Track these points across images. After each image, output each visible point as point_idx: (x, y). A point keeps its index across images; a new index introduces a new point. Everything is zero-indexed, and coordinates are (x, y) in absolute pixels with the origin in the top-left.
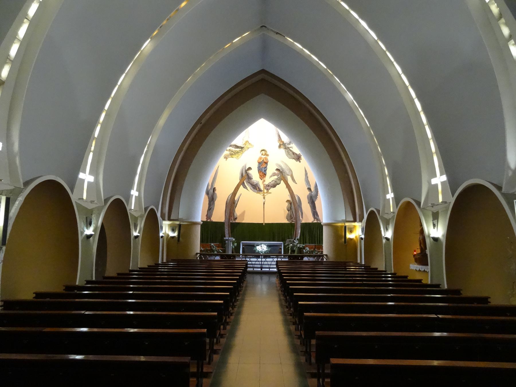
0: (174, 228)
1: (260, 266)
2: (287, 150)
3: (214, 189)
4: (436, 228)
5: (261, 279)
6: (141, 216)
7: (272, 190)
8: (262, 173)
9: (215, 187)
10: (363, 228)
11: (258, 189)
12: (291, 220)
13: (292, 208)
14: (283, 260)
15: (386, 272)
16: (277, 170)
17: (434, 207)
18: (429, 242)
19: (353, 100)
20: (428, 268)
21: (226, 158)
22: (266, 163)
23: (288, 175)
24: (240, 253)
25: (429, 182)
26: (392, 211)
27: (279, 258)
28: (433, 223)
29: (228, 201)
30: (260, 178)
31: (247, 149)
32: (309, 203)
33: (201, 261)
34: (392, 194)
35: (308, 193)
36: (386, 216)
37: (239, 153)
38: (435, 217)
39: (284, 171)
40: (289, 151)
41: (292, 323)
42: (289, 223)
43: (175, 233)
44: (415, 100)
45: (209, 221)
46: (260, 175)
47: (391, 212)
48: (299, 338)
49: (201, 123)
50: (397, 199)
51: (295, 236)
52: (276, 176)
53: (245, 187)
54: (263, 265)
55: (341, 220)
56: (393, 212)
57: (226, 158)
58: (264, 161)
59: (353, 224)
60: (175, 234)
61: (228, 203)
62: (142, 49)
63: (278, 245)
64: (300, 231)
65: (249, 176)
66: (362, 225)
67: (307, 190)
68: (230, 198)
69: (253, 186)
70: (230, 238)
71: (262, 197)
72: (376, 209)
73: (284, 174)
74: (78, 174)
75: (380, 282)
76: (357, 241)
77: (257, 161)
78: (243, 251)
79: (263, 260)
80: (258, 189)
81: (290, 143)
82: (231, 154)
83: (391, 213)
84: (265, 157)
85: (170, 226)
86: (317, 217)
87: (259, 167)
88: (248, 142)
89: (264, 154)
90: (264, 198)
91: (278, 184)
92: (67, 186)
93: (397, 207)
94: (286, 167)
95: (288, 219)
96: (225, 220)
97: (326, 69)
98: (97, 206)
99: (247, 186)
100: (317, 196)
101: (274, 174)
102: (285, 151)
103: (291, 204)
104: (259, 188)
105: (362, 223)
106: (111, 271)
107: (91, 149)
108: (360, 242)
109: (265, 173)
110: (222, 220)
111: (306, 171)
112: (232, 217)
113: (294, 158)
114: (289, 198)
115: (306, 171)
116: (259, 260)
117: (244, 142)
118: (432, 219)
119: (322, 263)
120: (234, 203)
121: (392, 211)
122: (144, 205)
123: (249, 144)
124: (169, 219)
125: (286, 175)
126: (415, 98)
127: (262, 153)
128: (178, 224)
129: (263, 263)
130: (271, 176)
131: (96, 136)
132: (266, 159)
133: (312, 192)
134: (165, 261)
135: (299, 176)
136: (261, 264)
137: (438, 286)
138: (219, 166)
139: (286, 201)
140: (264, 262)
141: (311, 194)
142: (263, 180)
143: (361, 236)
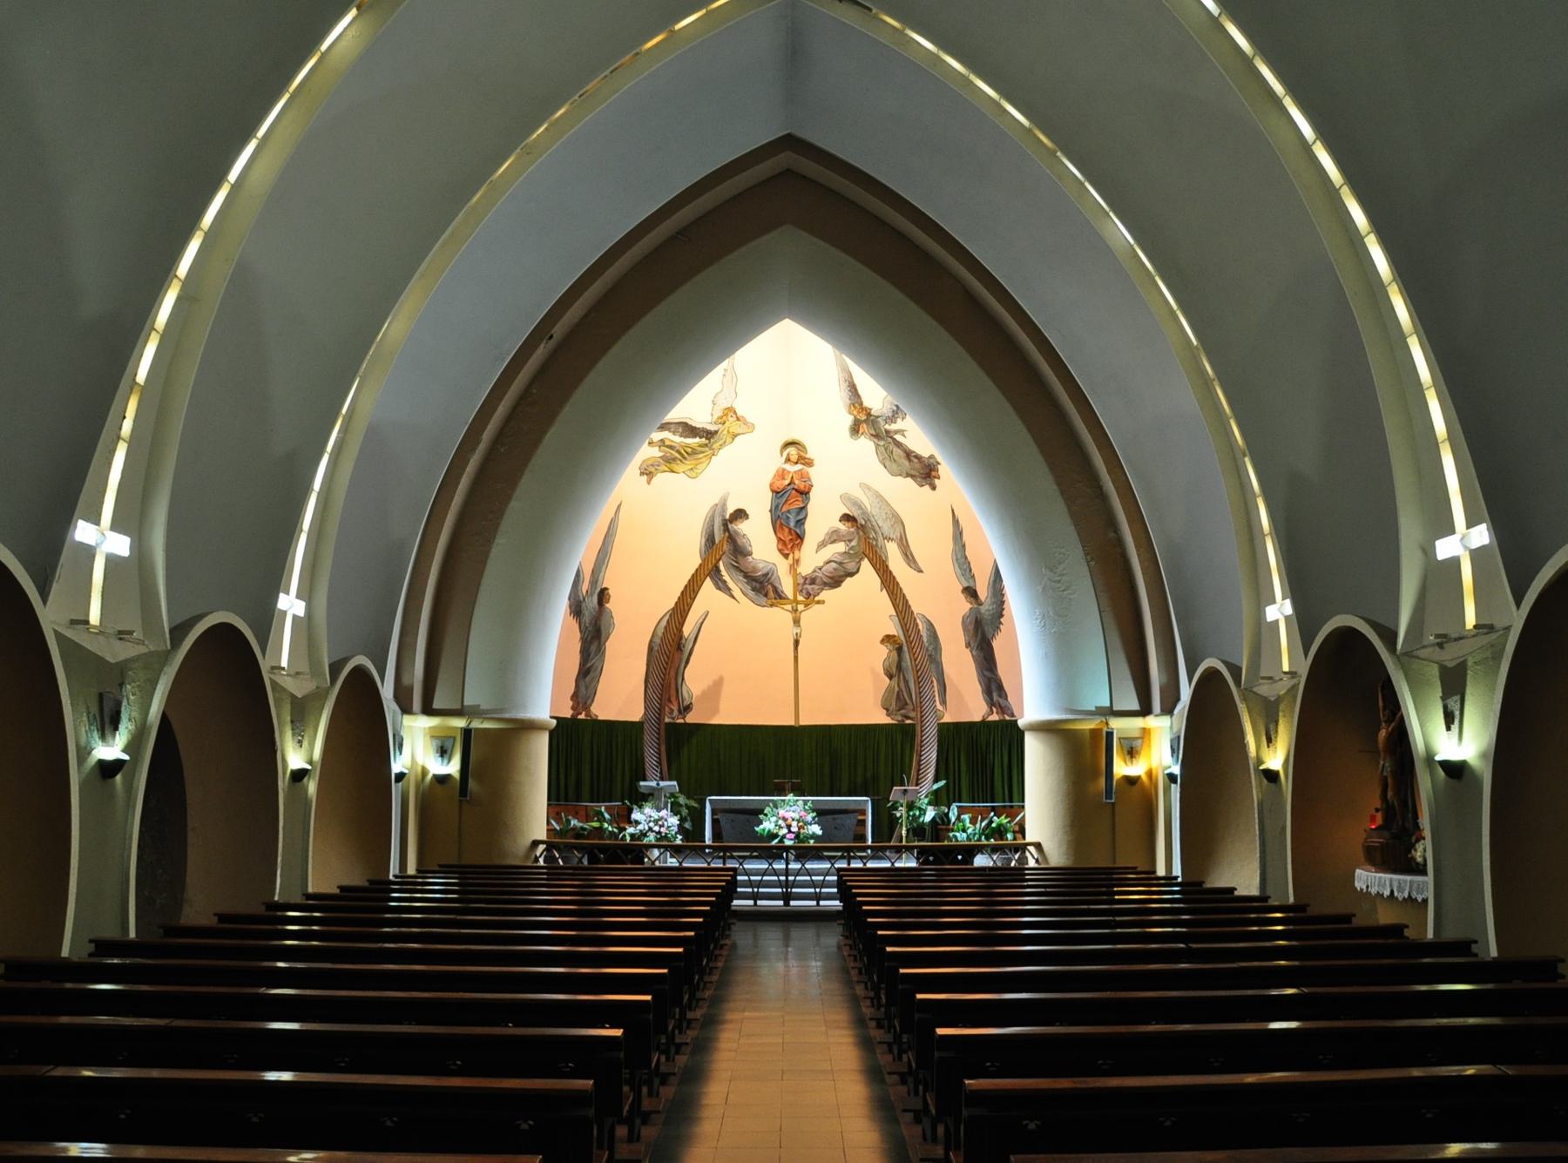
0: (448, 745)
1: (780, 890)
2: (882, 443)
3: (603, 595)
4: (1455, 727)
5: (787, 940)
6: (318, 696)
7: (826, 595)
8: (787, 530)
9: (604, 586)
10: (1179, 737)
11: (771, 594)
12: (902, 711)
13: (903, 664)
14: (870, 865)
15: (1267, 901)
16: (847, 518)
17: (1445, 645)
18: (1430, 785)
19: (1132, 246)
20: (1424, 887)
21: (648, 472)
22: (804, 493)
23: (890, 539)
24: (705, 842)
25: (1428, 551)
26: (1286, 668)
27: (854, 858)
28: (1445, 708)
29: (658, 640)
30: (780, 551)
31: (729, 440)
32: (968, 645)
33: (552, 869)
34: (1288, 602)
35: (967, 609)
36: (1264, 689)
37: (701, 456)
38: (1454, 685)
39: (874, 524)
40: (892, 446)
41: (912, 1114)
42: (895, 724)
43: (452, 762)
44: (1365, 240)
45: (582, 716)
46: (779, 539)
47: (1285, 673)
48: (918, 1120)
49: (551, 337)
50: (1305, 622)
51: (918, 775)
52: (843, 543)
53: (722, 586)
54: (795, 884)
55: (1094, 709)
56: (1292, 674)
57: (648, 472)
58: (796, 487)
59: (1138, 722)
60: (453, 768)
61: (656, 648)
62: (324, 47)
63: (852, 807)
64: (934, 755)
65: (739, 542)
66: (1174, 725)
67: (962, 597)
68: (666, 627)
69: (754, 584)
70: (662, 784)
71: (789, 617)
72: (1225, 663)
73: (872, 535)
74: (67, 523)
75: (1233, 903)
76: (1144, 778)
77: (768, 486)
78: (717, 835)
79: (794, 866)
80: (771, 594)
81: (893, 416)
82: (668, 460)
83: (1283, 675)
84: (800, 470)
85: (432, 737)
86: (1000, 700)
87: (777, 507)
88: (735, 413)
89: (794, 458)
90: (797, 622)
91: (851, 575)
92: (32, 585)
93: (1306, 655)
94: (880, 508)
95: (887, 710)
96: (645, 713)
97: (1029, 130)
98: (142, 650)
99: (731, 584)
100: (1002, 620)
101: (834, 537)
102: (877, 446)
103: (899, 650)
104: (776, 590)
105: (1174, 717)
106: (199, 909)
107: (120, 429)
108: (1167, 791)
109: (798, 531)
110: (633, 710)
111: (956, 522)
112: (673, 699)
113: (913, 473)
114: (893, 629)
115: (956, 522)
116: (775, 866)
117: (718, 413)
118: (1441, 695)
119: (1019, 873)
120: (679, 647)
121: (1286, 668)
122: (329, 657)
123: (738, 419)
124: (428, 710)
125: (880, 538)
126: (1368, 234)
127: (788, 455)
128: (461, 728)
129: (791, 878)
130: (822, 545)
131: (142, 376)
132: (804, 477)
133: (981, 604)
134: (411, 870)
135: (931, 543)
136: (787, 884)
137: (1464, 947)
138: (619, 506)
139: (880, 639)
140: (798, 873)
141: (978, 611)
142: (791, 557)
143: (1170, 767)
